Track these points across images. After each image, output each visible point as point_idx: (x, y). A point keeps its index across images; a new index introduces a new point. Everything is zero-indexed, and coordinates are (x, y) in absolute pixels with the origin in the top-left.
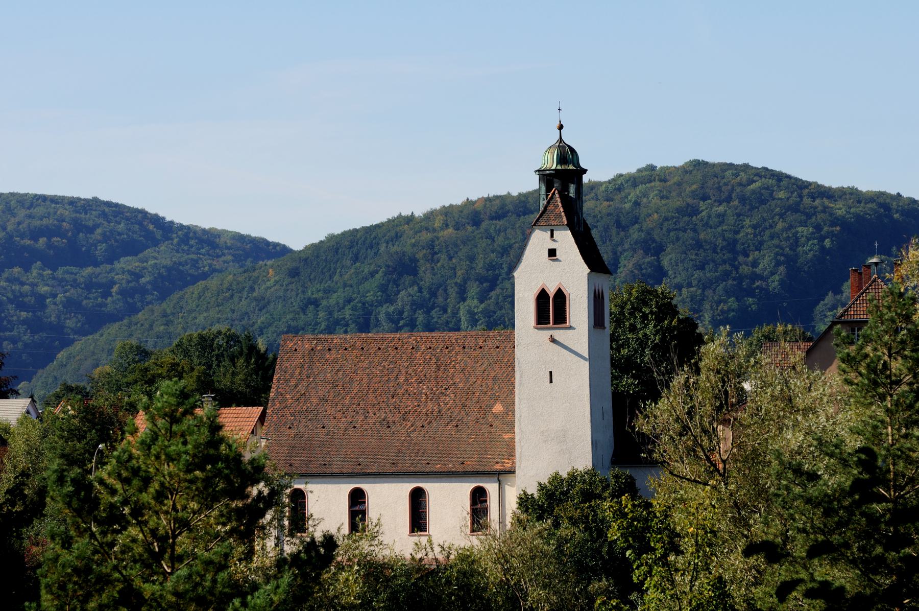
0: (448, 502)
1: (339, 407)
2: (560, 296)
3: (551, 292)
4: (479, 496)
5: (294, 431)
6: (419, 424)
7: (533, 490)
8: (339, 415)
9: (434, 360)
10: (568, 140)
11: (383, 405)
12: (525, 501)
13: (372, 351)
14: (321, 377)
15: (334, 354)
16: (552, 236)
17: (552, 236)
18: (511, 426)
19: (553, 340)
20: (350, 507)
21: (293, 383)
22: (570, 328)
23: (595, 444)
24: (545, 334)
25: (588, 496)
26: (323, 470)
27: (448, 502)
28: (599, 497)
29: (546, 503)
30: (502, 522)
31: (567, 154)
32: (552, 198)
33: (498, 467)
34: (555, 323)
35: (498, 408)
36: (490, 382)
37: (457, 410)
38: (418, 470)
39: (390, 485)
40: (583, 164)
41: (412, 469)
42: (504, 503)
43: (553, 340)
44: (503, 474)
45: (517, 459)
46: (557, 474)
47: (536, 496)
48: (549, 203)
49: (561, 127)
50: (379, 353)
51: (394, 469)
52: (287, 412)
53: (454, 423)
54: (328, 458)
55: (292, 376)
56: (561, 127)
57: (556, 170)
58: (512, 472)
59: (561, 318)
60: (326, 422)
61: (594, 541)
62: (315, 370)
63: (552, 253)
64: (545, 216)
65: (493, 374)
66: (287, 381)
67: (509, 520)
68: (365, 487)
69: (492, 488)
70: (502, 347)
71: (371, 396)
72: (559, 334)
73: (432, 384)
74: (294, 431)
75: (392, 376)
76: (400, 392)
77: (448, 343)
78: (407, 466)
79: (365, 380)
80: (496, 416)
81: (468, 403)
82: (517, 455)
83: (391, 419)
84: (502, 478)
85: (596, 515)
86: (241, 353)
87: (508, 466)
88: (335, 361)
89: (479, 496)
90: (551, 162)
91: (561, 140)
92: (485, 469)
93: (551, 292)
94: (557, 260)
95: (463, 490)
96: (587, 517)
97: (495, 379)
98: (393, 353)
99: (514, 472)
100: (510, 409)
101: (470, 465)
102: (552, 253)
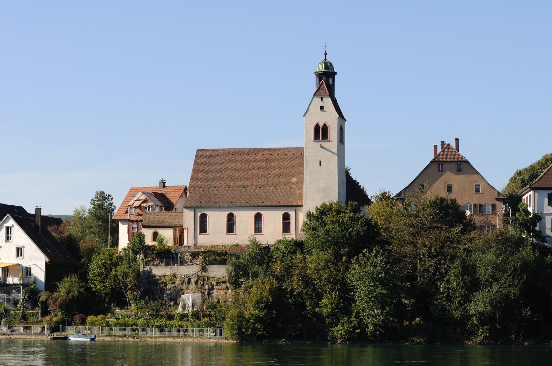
0: (272, 220)
1: (222, 179)
2: (325, 127)
3: (321, 125)
4: (286, 217)
5: (202, 189)
6: (258, 186)
7: (313, 211)
8: (222, 183)
9: (265, 160)
10: (329, 60)
11: (242, 178)
12: (309, 216)
13: (237, 156)
14: (214, 166)
15: (220, 157)
16: (322, 100)
17: (322, 100)
18: (301, 188)
19: (321, 147)
20: (227, 221)
21: (201, 169)
22: (329, 141)
23: (339, 194)
24: (318, 144)
25: (339, 212)
26: (215, 205)
27: (272, 220)
28: (344, 212)
29: (321, 215)
30: (296, 229)
31: (328, 66)
32: (322, 84)
33: (295, 204)
34: (322, 139)
35: (294, 180)
36: (291, 169)
37: (276, 180)
38: (259, 206)
39: (247, 212)
40: (335, 70)
41: (256, 204)
42: (299, 219)
43: (321, 147)
44: (297, 207)
45: (304, 201)
46: (324, 203)
47: (315, 213)
48: (320, 86)
49: (326, 54)
50: (240, 156)
51: (248, 204)
52: (199, 181)
53: (274, 186)
54: (217, 200)
55: (201, 166)
56: (326, 54)
57: (324, 72)
58: (301, 206)
59: (325, 137)
60: (216, 185)
61: (343, 231)
62: (212, 164)
63: (322, 108)
64: (319, 91)
65: (292, 166)
66: (199, 168)
67: (300, 227)
68: (234, 212)
69: (292, 214)
70: (296, 154)
71: (237, 175)
72: (324, 144)
73: (264, 170)
74: (202, 189)
75: (246, 167)
76: (250, 173)
77: (271, 153)
78: (254, 204)
79: (234, 168)
80: (293, 183)
81: (281, 178)
82: (304, 198)
83: (245, 184)
84: (297, 208)
85: (343, 220)
86: (118, 319)
87: (300, 203)
88: (221, 160)
89: (286, 217)
90: (321, 68)
91: (326, 59)
92: (288, 207)
93: (321, 125)
94: (324, 111)
95: (278, 215)
96: (339, 221)
97: (292, 167)
98: (246, 157)
99: (302, 206)
100: (301, 180)
101: (282, 203)
102: (322, 108)
